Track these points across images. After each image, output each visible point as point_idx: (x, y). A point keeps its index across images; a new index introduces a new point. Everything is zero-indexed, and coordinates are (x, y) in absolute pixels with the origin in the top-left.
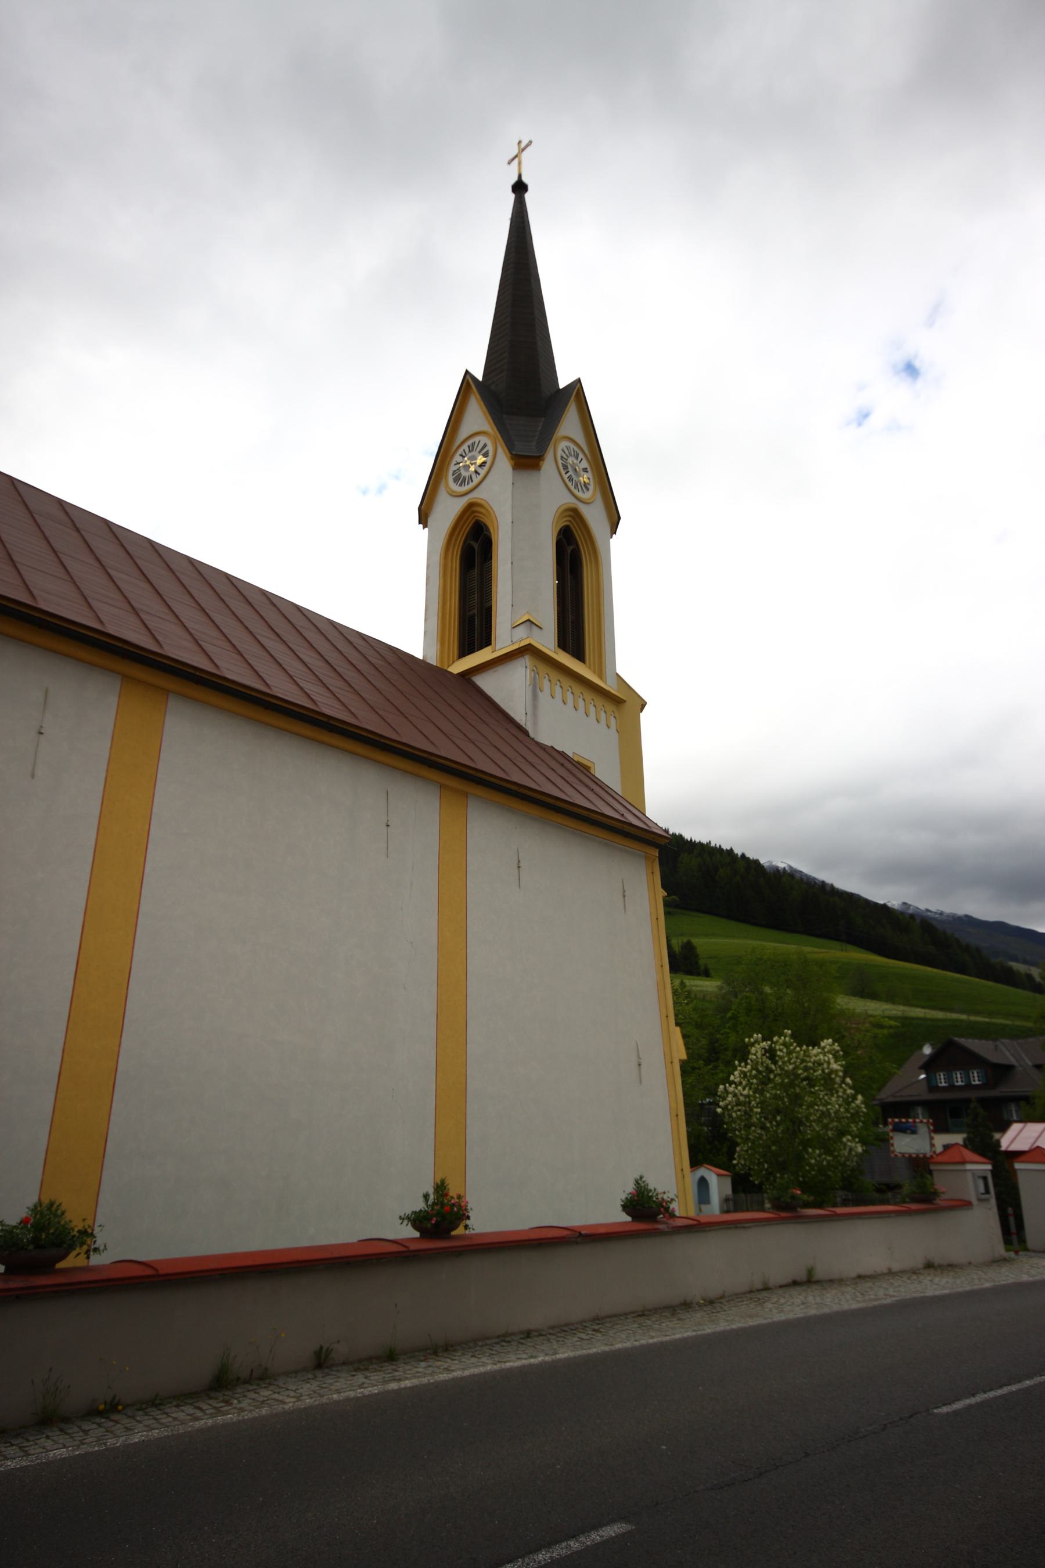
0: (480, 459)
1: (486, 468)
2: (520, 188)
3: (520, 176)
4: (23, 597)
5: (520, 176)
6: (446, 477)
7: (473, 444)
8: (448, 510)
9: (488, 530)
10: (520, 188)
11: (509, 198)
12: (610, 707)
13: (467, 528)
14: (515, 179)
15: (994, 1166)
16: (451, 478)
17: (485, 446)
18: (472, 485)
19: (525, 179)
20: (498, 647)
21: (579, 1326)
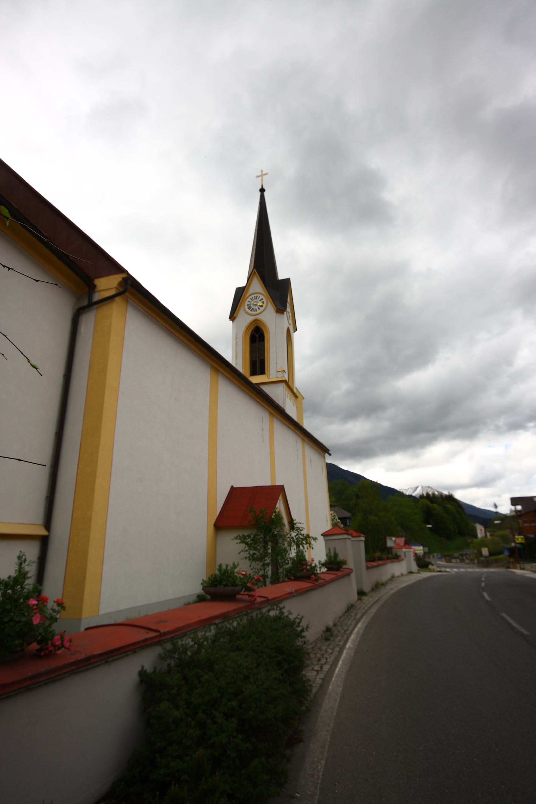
0: (260, 304)
1: (262, 309)
2: (262, 190)
3: (262, 186)
4: (282, 406)
5: (262, 186)
6: (244, 305)
7: (257, 297)
8: (245, 319)
9: (262, 330)
10: (262, 190)
11: (259, 194)
12: (294, 398)
13: (253, 328)
14: (260, 187)
15: (366, 538)
16: (246, 307)
17: (262, 299)
18: (256, 313)
19: (264, 187)
20: (271, 377)
21: (295, 594)
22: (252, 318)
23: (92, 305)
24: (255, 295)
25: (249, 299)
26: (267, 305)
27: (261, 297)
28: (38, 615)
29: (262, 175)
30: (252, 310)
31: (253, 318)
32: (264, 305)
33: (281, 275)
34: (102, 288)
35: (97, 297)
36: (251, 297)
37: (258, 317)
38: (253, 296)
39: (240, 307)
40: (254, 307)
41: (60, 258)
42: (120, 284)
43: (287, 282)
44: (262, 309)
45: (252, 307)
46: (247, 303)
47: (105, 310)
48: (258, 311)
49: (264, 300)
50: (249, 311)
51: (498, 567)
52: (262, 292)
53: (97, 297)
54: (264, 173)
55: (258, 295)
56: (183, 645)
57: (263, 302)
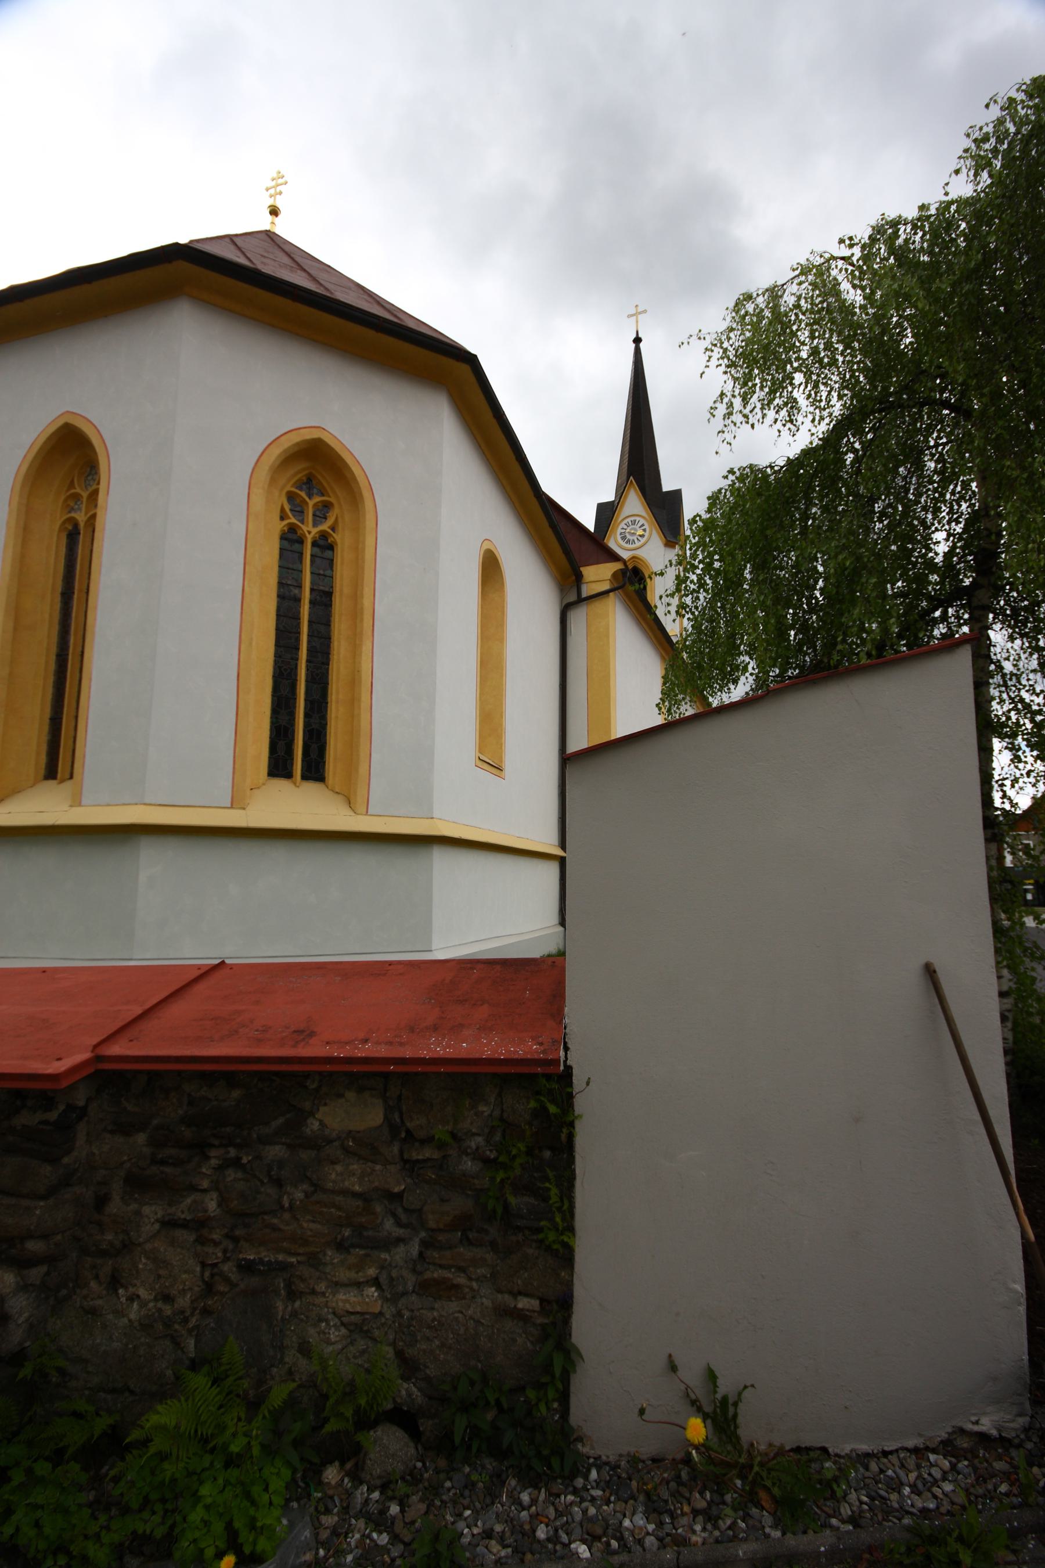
1: (643, 540)
2: (637, 340)
10: (637, 340)
11: (632, 346)
14: (634, 336)
16: (619, 537)
23: (580, 600)
24: (632, 519)
25: (623, 525)
26: (651, 534)
27: (642, 521)
29: (637, 314)
30: (628, 542)
32: (647, 534)
33: (667, 486)
34: (592, 579)
35: (586, 591)
36: (625, 521)
38: (629, 520)
39: (610, 537)
40: (631, 538)
42: (615, 575)
43: (677, 495)
44: (643, 540)
45: (628, 537)
46: (619, 531)
47: (598, 606)
48: (638, 544)
49: (646, 526)
50: (621, 542)
52: (644, 514)
53: (586, 591)
54: (640, 309)
55: (638, 519)
57: (644, 530)
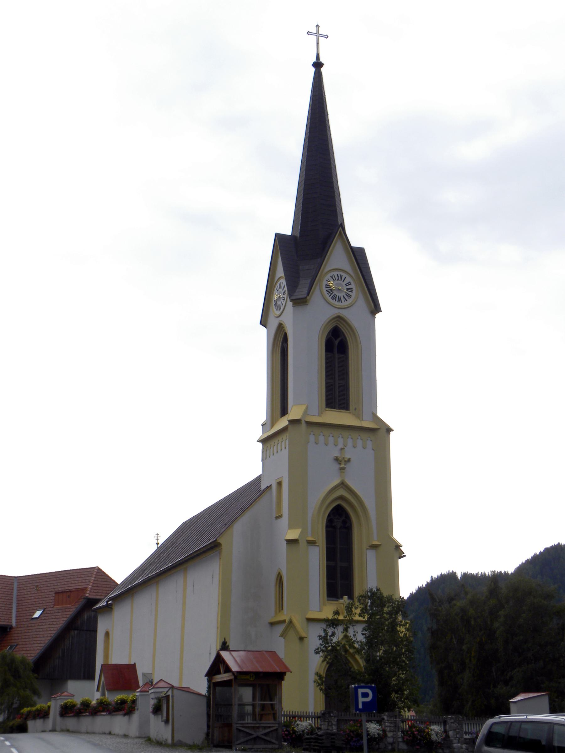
2: (318, 65)
14: (314, 60)
16: (324, 290)
17: (349, 284)
19: (322, 60)
22: (334, 312)
24: (339, 273)
25: (328, 277)
27: (348, 279)
28: (350, 686)
31: (336, 312)
36: (332, 274)
37: (345, 313)
38: (335, 273)
41: (311, 288)
46: (325, 283)
51: (481, 739)
55: (344, 275)
56: (424, 731)
